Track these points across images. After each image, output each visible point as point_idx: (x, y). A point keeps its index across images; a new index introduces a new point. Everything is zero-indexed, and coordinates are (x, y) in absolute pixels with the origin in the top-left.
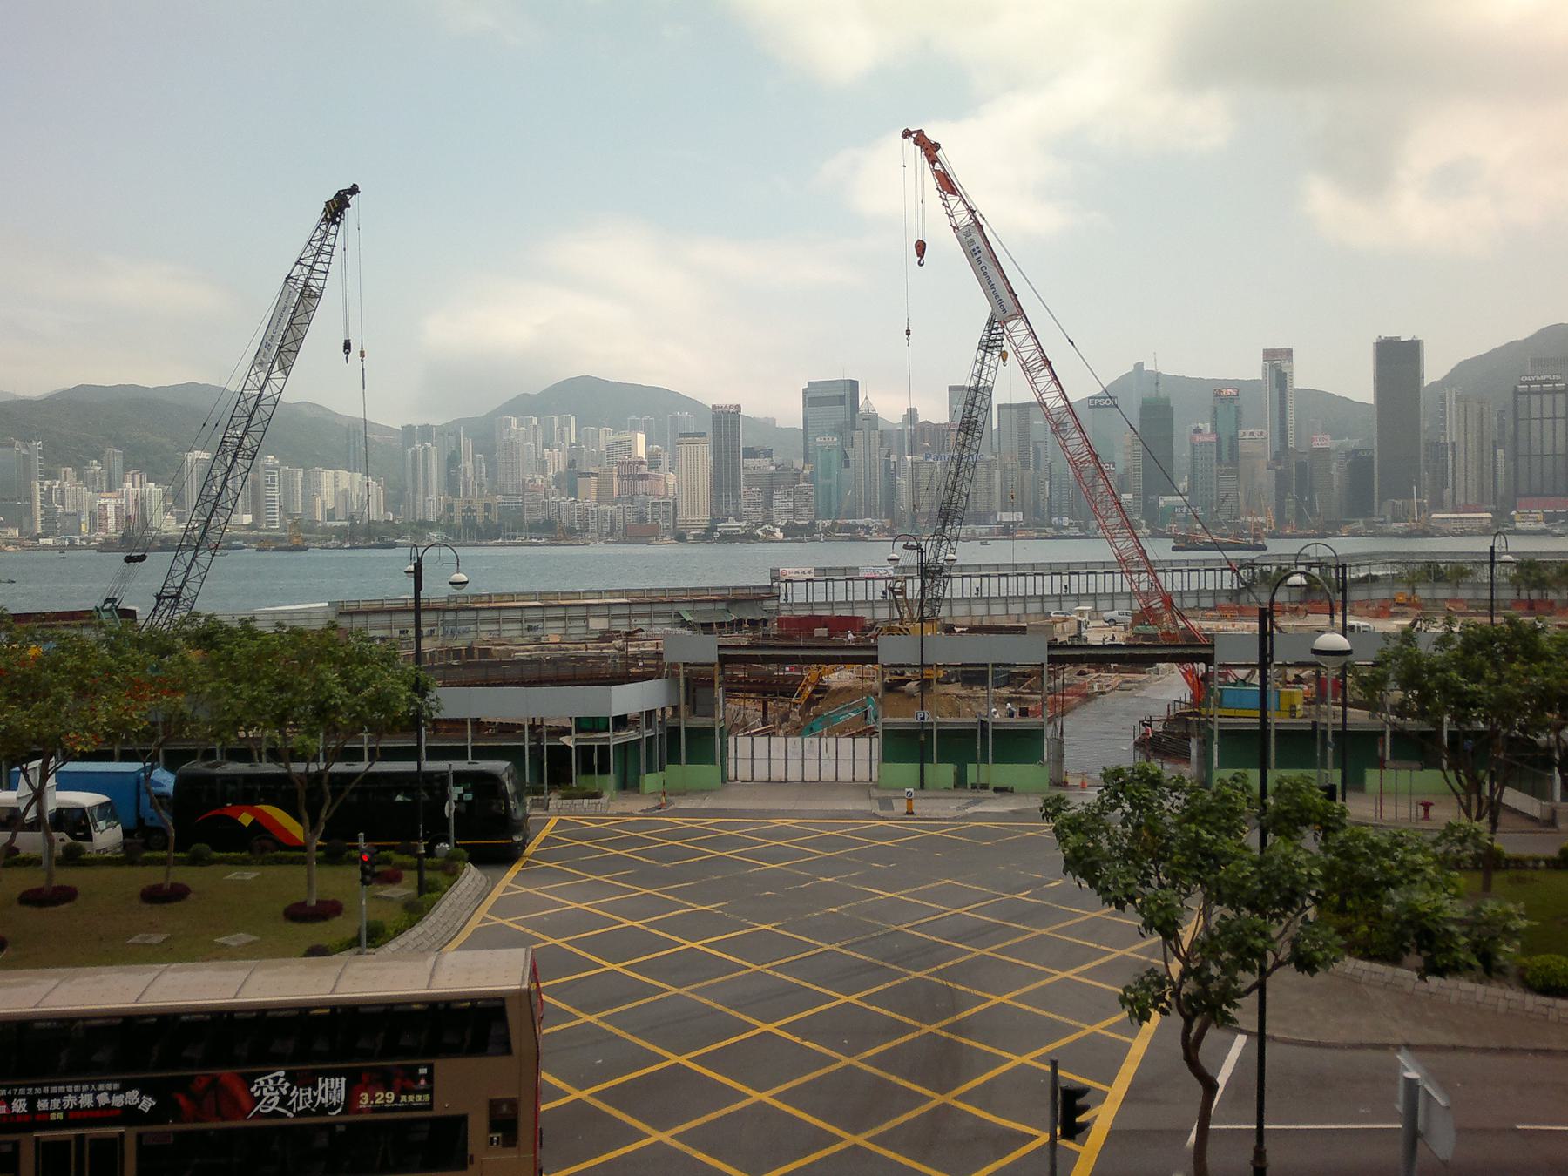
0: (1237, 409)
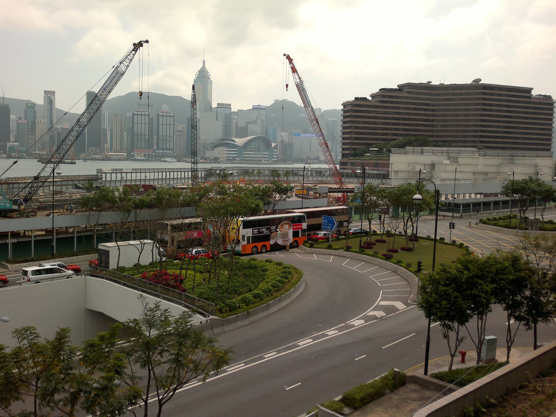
0: (35, 112)
